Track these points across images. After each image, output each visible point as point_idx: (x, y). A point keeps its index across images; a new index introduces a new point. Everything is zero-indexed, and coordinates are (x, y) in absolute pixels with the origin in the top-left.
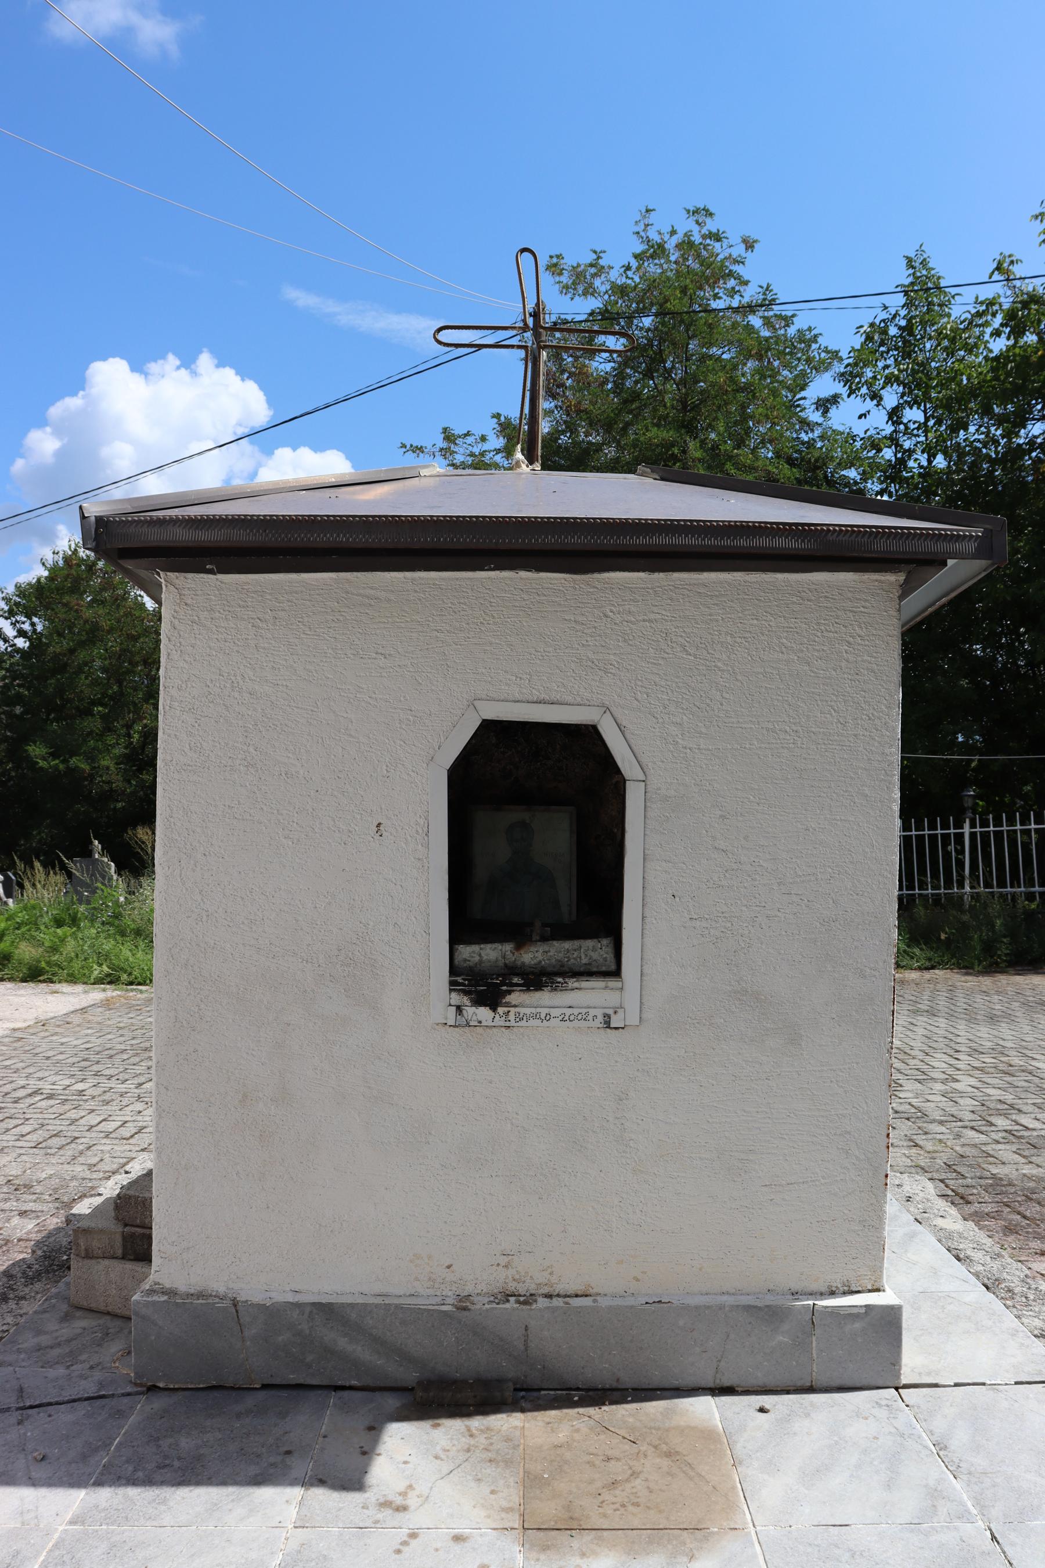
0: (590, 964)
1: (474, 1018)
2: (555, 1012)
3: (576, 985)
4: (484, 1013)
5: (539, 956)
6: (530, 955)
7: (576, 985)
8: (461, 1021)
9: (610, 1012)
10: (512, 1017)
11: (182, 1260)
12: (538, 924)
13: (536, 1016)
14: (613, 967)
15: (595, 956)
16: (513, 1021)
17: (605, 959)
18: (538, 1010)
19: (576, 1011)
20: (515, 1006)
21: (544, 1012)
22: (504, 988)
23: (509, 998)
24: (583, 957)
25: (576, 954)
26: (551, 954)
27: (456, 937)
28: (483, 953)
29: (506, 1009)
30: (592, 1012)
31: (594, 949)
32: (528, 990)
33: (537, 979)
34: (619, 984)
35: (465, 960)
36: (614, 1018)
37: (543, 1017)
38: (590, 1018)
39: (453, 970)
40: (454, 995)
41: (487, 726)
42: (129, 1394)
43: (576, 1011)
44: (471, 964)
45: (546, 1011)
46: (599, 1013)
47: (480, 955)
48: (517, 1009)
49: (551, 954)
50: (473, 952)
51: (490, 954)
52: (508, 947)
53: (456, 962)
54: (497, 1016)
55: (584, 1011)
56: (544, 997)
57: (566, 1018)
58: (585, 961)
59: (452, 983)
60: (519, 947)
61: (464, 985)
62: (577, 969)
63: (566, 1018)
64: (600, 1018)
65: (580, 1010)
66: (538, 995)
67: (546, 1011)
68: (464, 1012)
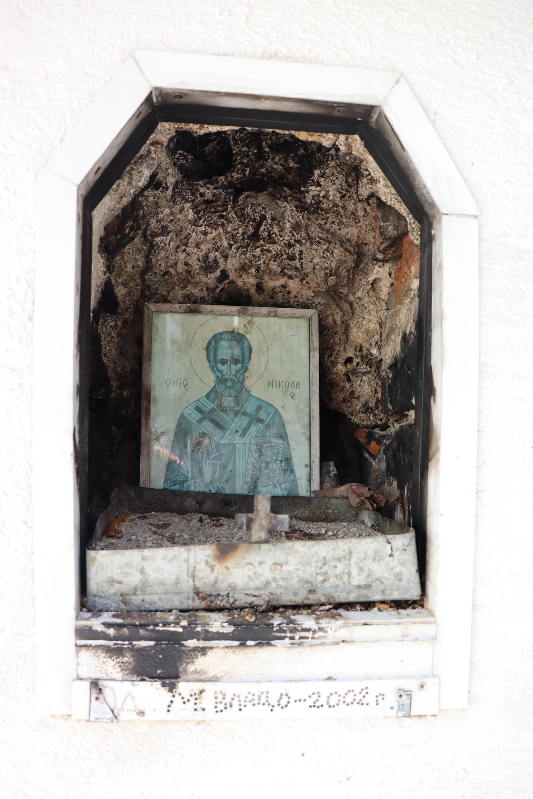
0: (368, 587)
1: (129, 704)
2: (297, 691)
3: (343, 633)
4: (151, 692)
5: (266, 573)
6: (248, 571)
7: (343, 633)
8: (100, 709)
9: (411, 685)
10: (208, 700)
11: (389, 606)
12: (263, 505)
13: (259, 700)
14: (414, 593)
15: (379, 570)
16: (210, 710)
17: (399, 577)
18: (264, 687)
19: (341, 687)
20: (215, 679)
21: (275, 691)
22: (192, 643)
23: (200, 663)
24: (355, 572)
25: (340, 568)
26: (290, 568)
27: (96, 526)
28: (149, 567)
29: (196, 687)
30: (375, 688)
31: (377, 558)
32: (243, 645)
33: (259, 622)
34: (429, 630)
35: (112, 582)
36: (417, 695)
37: (273, 701)
38: (371, 699)
39: (85, 600)
40: (85, 654)
41: (162, 107)
42: (188, 570)
43: (341, 687)
44: (124, 588)
45: (282, 688)
46: (390, 689)
47: (142, 571)
48: (219, 687)
49: (290, 568)
50: (129, 565)
51: (157, 569)
52: (201, 555)
53: (93, 585)
54: (178, 700)
55: (358, 686)
56: (275, 660)
57: (322, 701)
58: (358, 579)
59: (84, 633)
60: (225, 551)
61: (106, 637)
62: (342, 598)
63: (322, 701)
64: (392, 699)
65: (350, 685)
66: (263, 654)
67: (282, 688)
68: (106, 691)
